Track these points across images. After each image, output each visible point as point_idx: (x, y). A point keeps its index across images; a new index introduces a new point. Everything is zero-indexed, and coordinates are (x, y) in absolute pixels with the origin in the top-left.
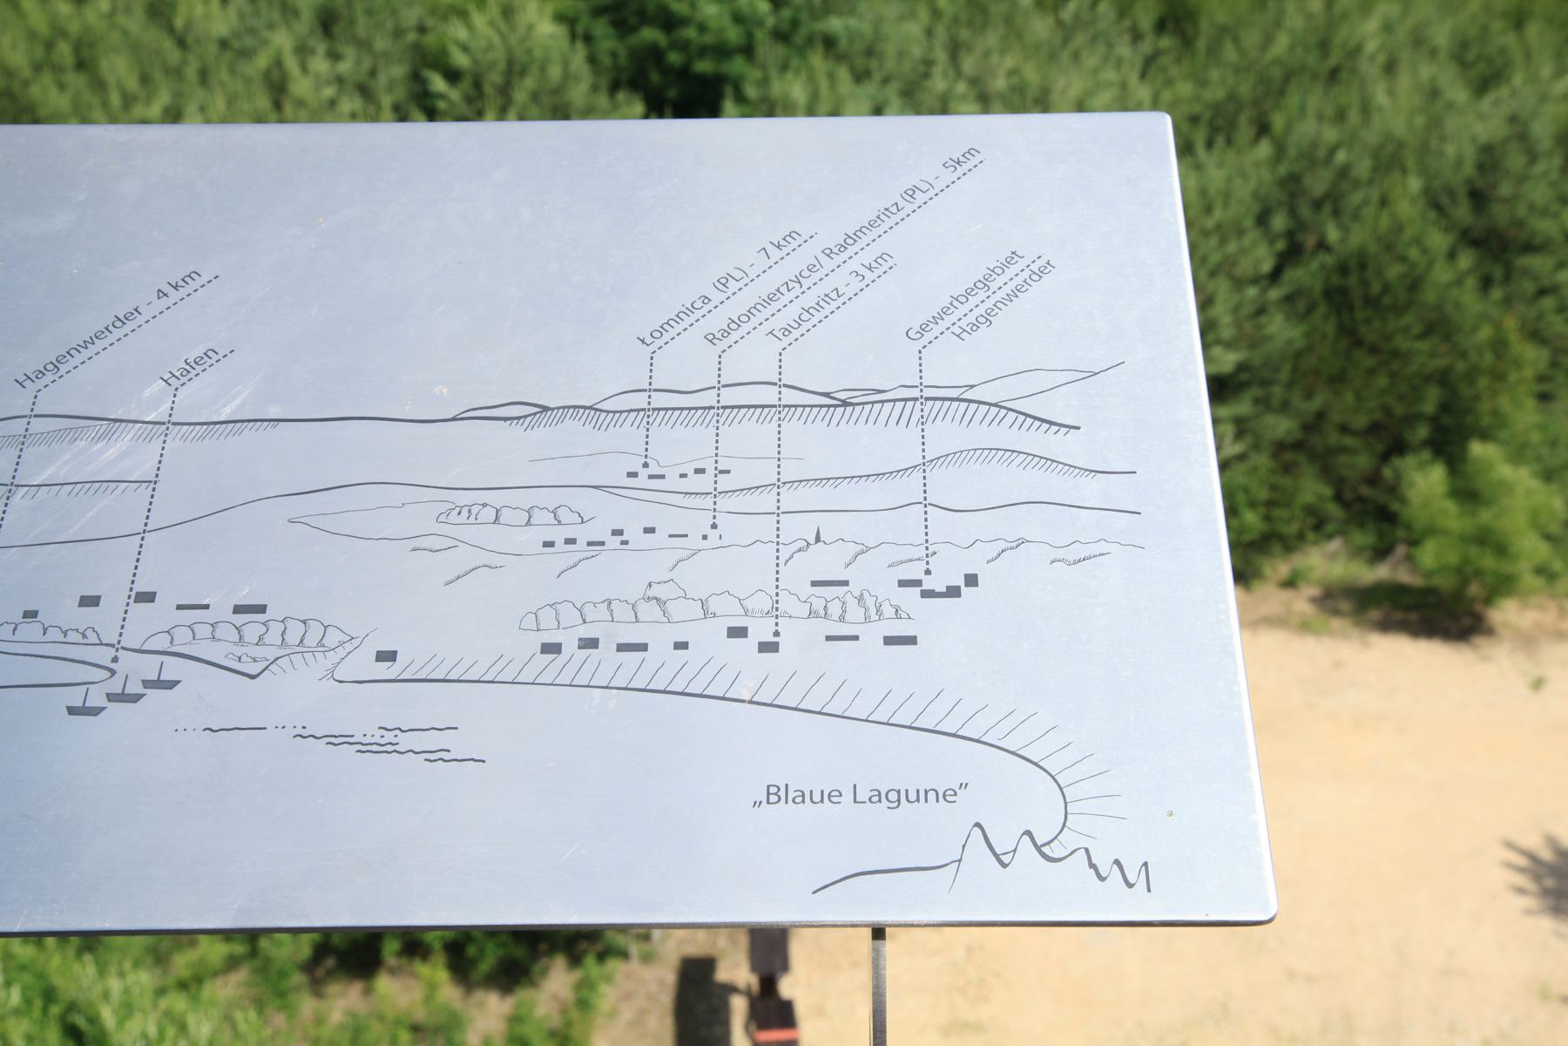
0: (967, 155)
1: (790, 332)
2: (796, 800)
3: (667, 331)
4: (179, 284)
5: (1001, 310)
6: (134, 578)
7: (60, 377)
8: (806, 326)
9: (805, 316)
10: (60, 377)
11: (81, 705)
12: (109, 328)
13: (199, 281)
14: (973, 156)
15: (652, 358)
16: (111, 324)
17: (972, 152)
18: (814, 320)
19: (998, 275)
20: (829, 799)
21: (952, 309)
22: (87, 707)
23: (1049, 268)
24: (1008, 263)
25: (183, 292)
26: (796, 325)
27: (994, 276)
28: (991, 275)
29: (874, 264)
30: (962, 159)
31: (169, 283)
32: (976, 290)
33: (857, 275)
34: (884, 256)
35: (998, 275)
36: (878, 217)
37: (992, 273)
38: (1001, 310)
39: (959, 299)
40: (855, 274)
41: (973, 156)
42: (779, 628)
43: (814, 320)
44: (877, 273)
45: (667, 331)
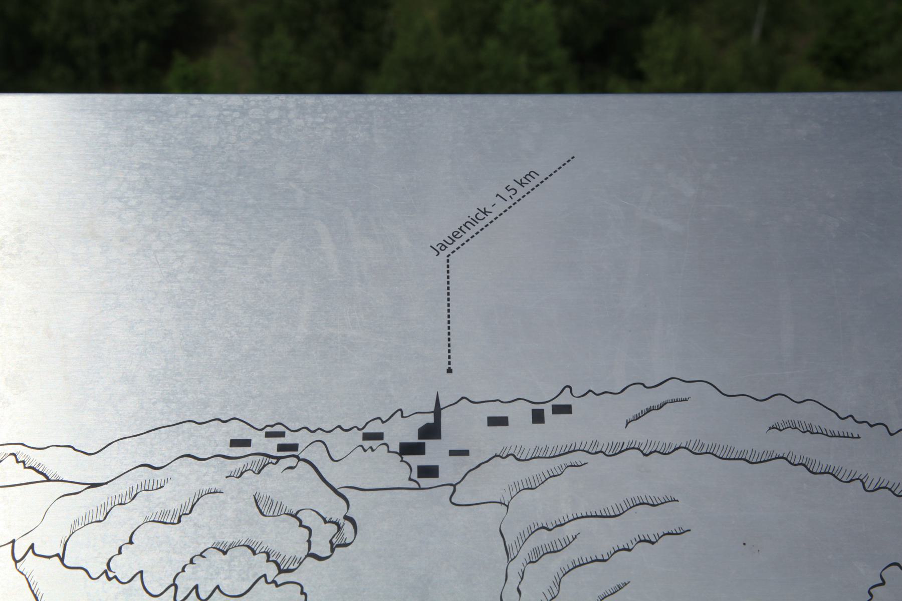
0: (528, 177)
1: (446, 247)
2: (514, 192)
3: (449, 237)
4: (523, 182)
5: (465, 233)
6: (503, 213)
9: (481, 216)
11: (433, 414)
13: (538, 180)
14: (847, 433)
15: (448, 261)
17: (532, 174)
20: (456, 238)
21: (461, 233)
22: (400, 451)
24: (455, 237)
25: (528, 188)
26: (450, 242)
29: (524, 181)
30: (524, 181)
31: (491, 212)
34: (532, 174)
36: (460, 229)
38: (465, 233)
41: (847, 433)
42: (451, 366)
45: (449, 237)
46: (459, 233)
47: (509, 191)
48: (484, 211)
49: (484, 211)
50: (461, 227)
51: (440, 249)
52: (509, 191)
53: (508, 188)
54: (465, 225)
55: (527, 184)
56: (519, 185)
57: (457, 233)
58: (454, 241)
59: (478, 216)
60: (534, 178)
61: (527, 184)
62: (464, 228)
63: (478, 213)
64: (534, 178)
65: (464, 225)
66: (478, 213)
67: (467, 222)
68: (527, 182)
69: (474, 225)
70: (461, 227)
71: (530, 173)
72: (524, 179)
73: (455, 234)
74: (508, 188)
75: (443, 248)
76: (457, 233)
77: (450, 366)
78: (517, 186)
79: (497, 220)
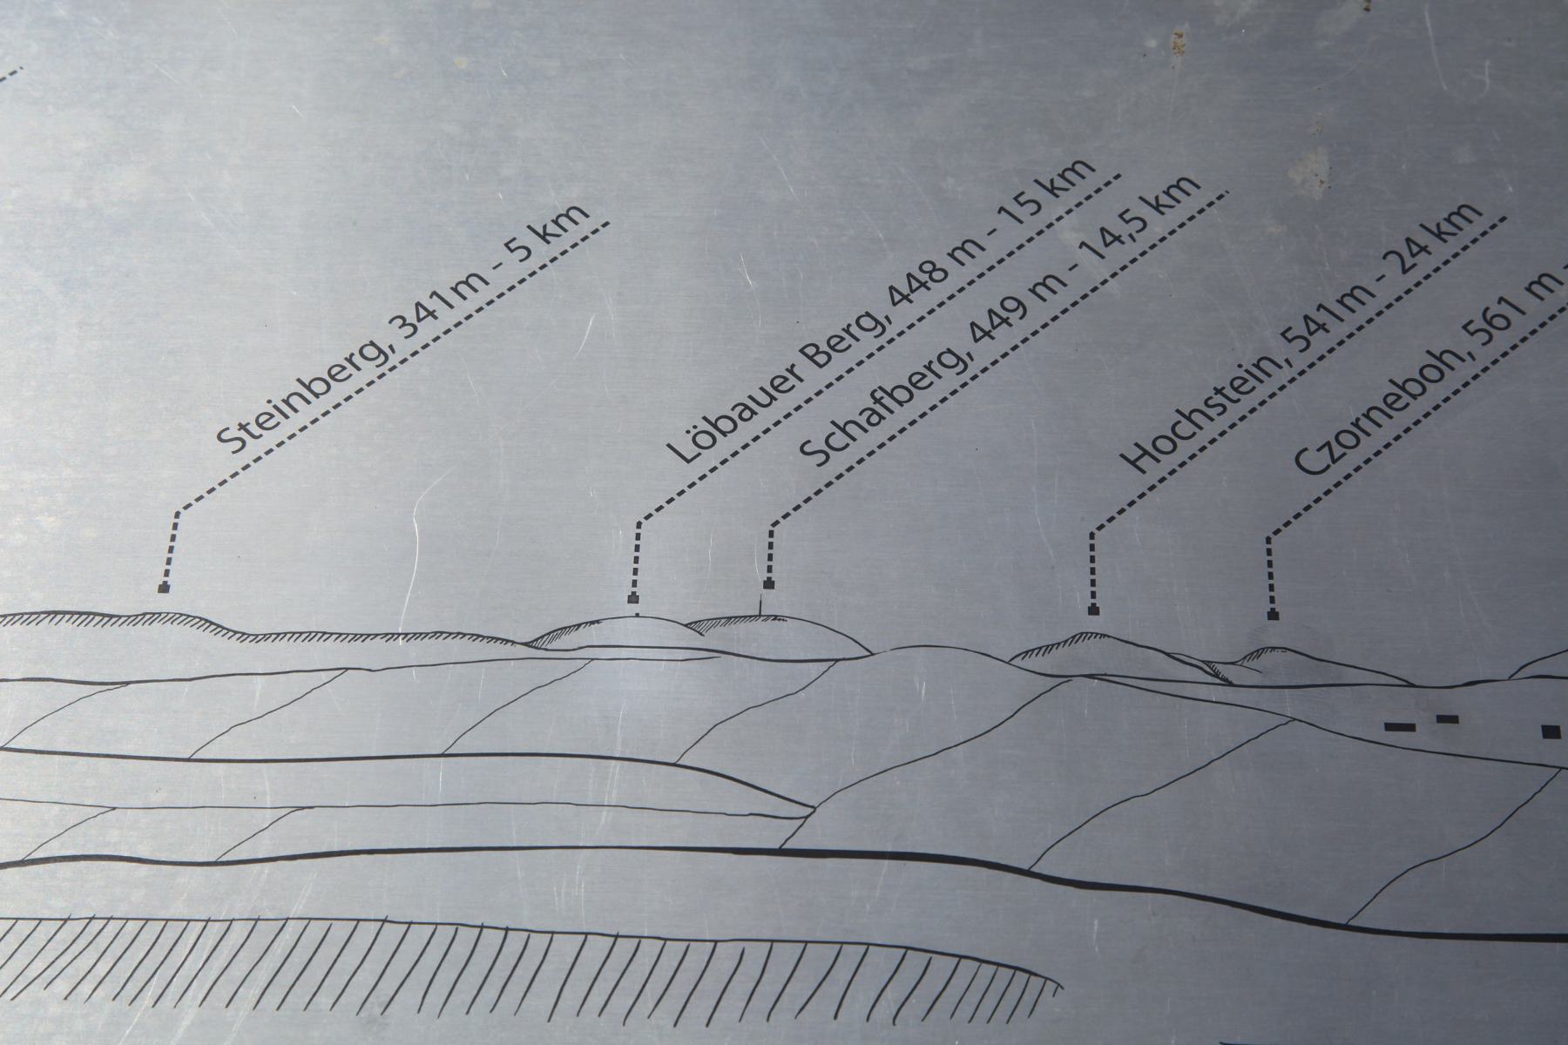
0: (1174, 192)
1: (754, 413)
4: (548, 231)
7: (391, 370)
8: (1185, 449)
9: (1185, 428)
10: (391, 370)
12: (851, 330)
16: (853, 323)
18: (1202, 438)
19: (1414, 397)
23: (792, 381)
24: (776, 388)
25: (556, 246)
26: (766, 400)
27: (1406, 398)
28: (1399, 397)
32: (735, 415)
33: (404, 325)
35: (1414, 397)
37: (1400, 392)
39: (847, 428)
40: (400, 322)
42: (169, 580)
43: (1202, 438)
44: (469, 306)
45: (1368, 434)
46: (786, 379)
47: (1127, 222)
48: (1050, 187)
49: (1050, 187)
50: (1358, 419)
51: (868, 421)
52: (1127, 222)
53: (1287, 335)
54: (1367, 416)
55: (558, 236)
56: (1154, 211)
57: (920, 377)
58: (773, 398)
59: (1177, 429)
60: (1083, 177)
61: (558, 236)
62: (1364, 423)
63: (1179, 422)
64: (1083, 177)
65: (1363, 415)
66: (1179, 422)
67: (967, 241)
68: (1066, 185)
69: (308, 402)
70: (1358, 419)
71: (963, 244)
72: (1446, 223)
73: (777, 382)
74: (1287, 335)
75: (875, 419)
76: (920, 377)
77: (166, 579)
78: (1042, 195)
79: (509, 286)
